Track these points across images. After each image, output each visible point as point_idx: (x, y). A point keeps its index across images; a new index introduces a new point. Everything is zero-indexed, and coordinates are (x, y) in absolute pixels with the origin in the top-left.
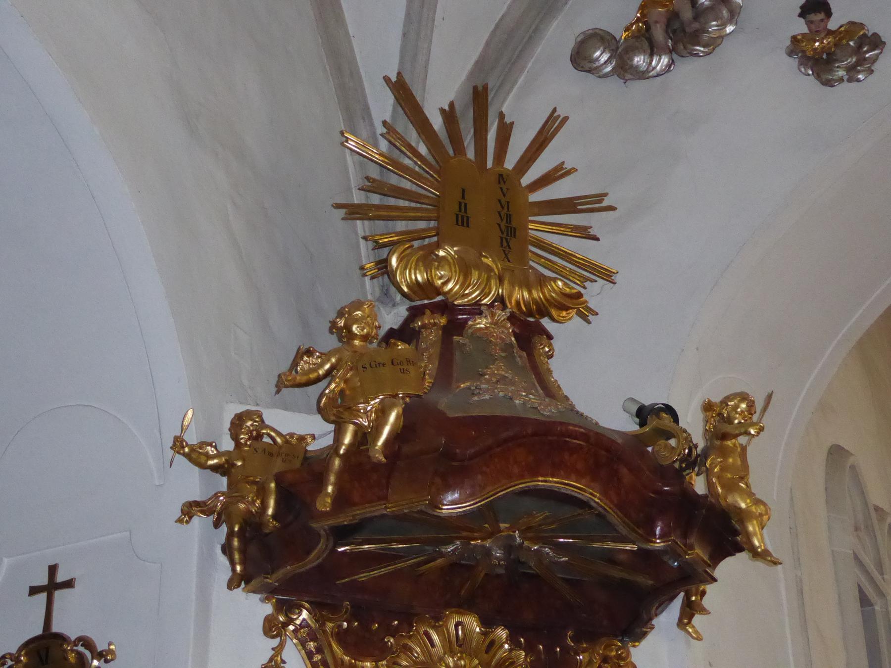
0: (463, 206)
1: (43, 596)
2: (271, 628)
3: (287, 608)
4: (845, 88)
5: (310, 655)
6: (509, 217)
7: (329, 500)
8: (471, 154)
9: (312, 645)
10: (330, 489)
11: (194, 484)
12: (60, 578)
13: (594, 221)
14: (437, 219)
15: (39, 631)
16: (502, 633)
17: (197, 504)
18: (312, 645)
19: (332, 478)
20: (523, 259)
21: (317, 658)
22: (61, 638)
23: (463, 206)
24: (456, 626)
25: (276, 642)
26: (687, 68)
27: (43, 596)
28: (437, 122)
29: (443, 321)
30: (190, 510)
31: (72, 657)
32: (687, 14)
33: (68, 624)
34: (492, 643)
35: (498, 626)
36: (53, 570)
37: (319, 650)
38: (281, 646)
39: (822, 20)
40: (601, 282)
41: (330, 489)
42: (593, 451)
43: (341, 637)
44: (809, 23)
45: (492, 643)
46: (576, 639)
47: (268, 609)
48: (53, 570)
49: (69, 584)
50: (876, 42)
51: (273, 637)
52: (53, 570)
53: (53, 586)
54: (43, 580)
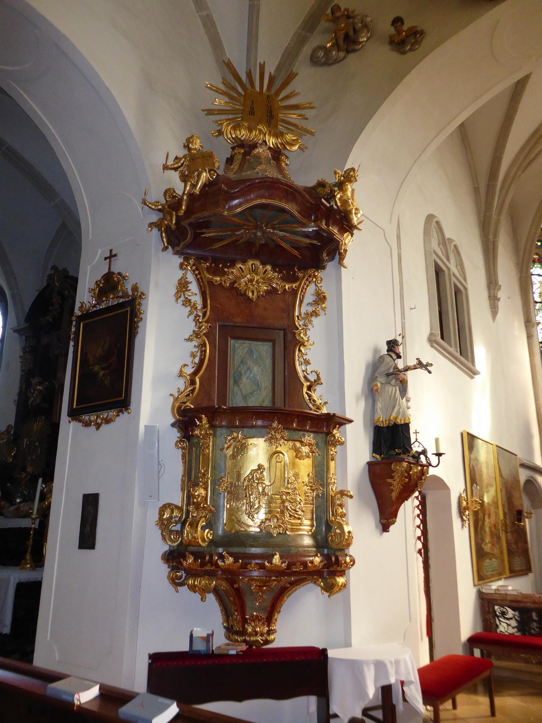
0: (252, 108)
1: (108, 260)
2: (181, 266)
3: (186, 259)
4: (410, 54)
5: (196, 275)
6: (271, 112)
7: (183, 212)
8: (258, 89)
9: (197, 272)
10: (184, 207)
11: (155, 217)
12: (114, 253)
13: (308, 113)
14: (242, 114)
15: (107, 271)
16: (269, 267)
17: (153, 223)
18: (197, 272)
19: (184, 203)
20: (276, 127)
21: (199, 276)
22: (113, 273)
23: (252, 108)
24: (252, 265)
25: (184, 272)
26: (352, 56)
27: (108, 260)
28: (244, 77)
29: (242, 151)
30: (151, 225)
31: (115, 279)
32: (351, 33)
33: (115, 269)
34: (266, 271)
35: (268, 264)
36: (111, 251)
37: (199, 274)
38: (186, 273)
39: (400, 26)
40: (308, 135)
41: (184, 207)
42: (291, 192)
43: (208, 269)
44: (396, 28)
45: (266, 271)
46: (299, 269)
47: (181, 260)
48: (111, 251)
49: (115, 255)
50: (422, 33)
51: (183, 270)
52: (111, 251)
53: (111, 256)
54: (108, 255)
